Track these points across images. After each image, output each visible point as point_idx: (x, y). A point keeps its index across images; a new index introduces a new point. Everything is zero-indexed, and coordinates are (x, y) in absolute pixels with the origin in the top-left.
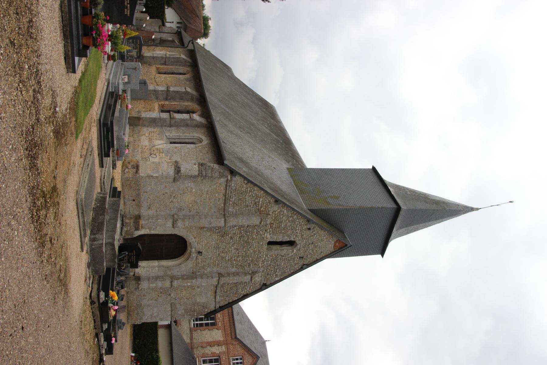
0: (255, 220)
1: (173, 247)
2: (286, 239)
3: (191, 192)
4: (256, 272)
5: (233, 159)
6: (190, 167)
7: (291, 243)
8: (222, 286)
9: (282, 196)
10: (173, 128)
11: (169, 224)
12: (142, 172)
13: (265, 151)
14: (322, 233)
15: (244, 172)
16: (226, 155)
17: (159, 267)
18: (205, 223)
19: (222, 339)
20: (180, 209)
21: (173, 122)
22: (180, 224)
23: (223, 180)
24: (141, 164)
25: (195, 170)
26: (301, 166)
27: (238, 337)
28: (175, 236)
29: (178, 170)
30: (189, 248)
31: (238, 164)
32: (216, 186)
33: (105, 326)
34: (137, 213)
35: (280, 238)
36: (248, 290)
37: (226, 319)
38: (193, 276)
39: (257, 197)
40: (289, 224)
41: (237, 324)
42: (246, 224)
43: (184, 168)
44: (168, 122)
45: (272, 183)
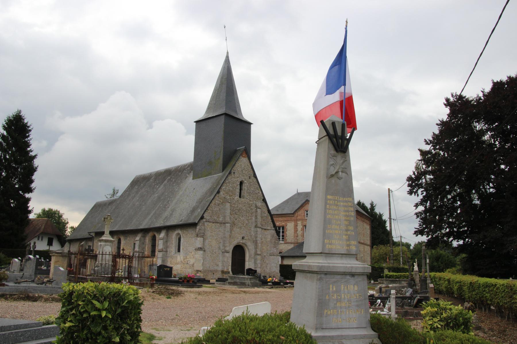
0: (228, 205)
1: (239, 252)
2: (239, 187)
3: (210, 242)
4: (256, 205)
5: (193, 217)
6: (199, 242)
7: (241, 183)
8: (262, 225)
9: (215, 188)
10: (168, 250)
11: (227, 255)
12: (201, 268)
13: (181, 193)
14: (237, 165)
15: (201, 211)
16: (191, 221)
17: (249, 261)
18: (227, 234)
19: (293, 223)
20: (219, 248)
21: (164, 250)
22: (227, 249)
23: (206, 224)
24: (196, 269)
25: (200, 239)
26: (189, 166)
27: (292, 212)
28: (233, 251)
29: (200, 249)
30: (240, 244)
31: (196, 214)
32: (208, 227)
33: (282, 284)
34: (220, 272)
35: (238, 190)
36: (266, 210)
37: (280, 219)
38: (255, 242)
39: (215, 204)
40: (231, 185)
41: (284, 213)
42: (229, 211)
43: (199, 245)
44: (164, 253)
45: (206, 193)
